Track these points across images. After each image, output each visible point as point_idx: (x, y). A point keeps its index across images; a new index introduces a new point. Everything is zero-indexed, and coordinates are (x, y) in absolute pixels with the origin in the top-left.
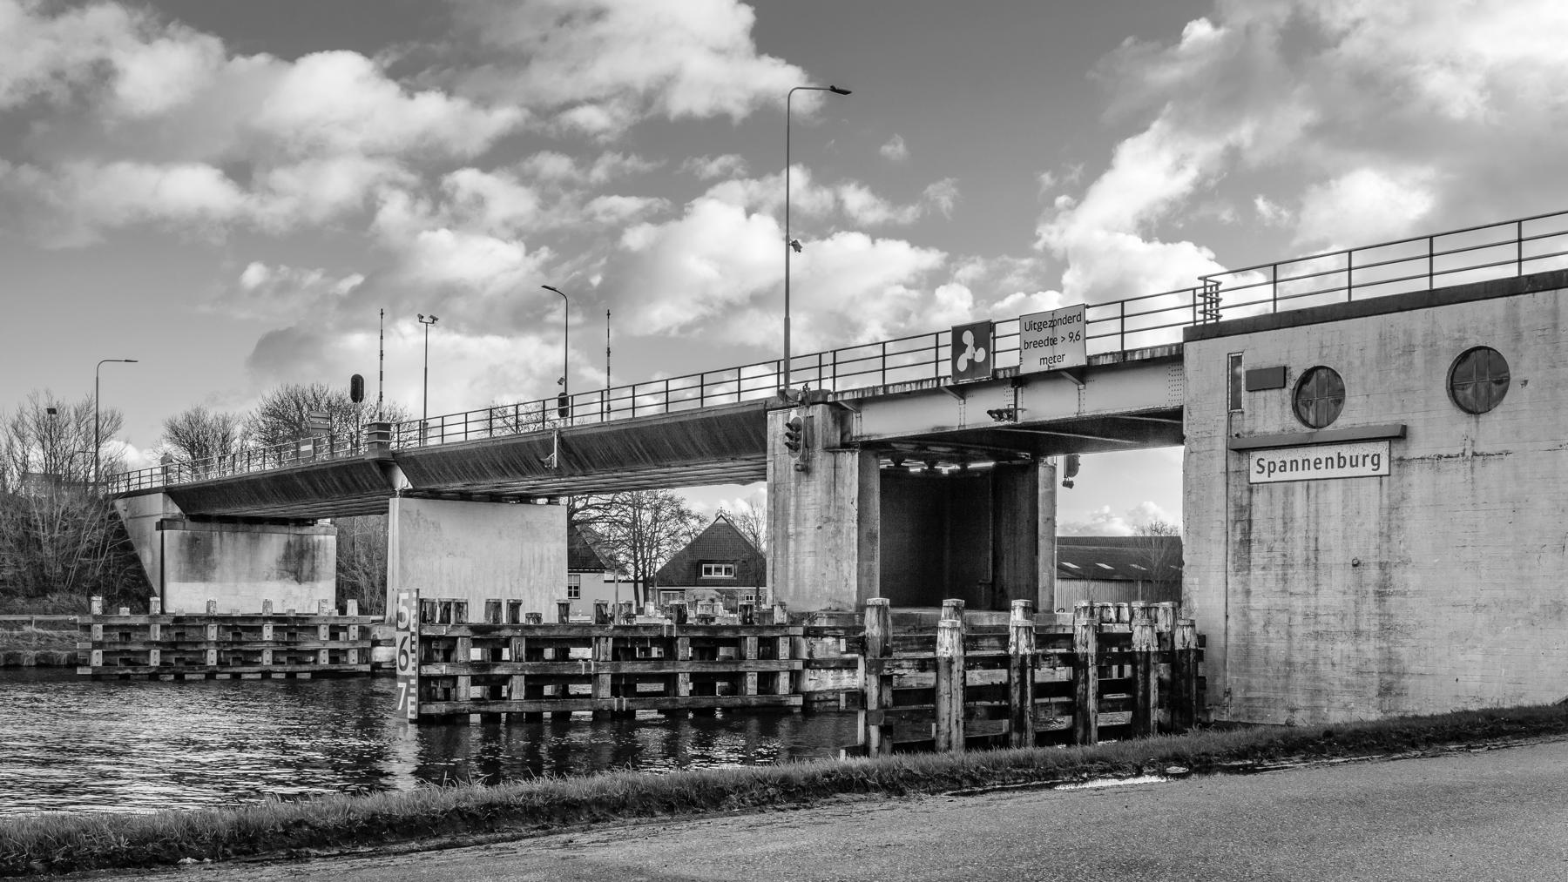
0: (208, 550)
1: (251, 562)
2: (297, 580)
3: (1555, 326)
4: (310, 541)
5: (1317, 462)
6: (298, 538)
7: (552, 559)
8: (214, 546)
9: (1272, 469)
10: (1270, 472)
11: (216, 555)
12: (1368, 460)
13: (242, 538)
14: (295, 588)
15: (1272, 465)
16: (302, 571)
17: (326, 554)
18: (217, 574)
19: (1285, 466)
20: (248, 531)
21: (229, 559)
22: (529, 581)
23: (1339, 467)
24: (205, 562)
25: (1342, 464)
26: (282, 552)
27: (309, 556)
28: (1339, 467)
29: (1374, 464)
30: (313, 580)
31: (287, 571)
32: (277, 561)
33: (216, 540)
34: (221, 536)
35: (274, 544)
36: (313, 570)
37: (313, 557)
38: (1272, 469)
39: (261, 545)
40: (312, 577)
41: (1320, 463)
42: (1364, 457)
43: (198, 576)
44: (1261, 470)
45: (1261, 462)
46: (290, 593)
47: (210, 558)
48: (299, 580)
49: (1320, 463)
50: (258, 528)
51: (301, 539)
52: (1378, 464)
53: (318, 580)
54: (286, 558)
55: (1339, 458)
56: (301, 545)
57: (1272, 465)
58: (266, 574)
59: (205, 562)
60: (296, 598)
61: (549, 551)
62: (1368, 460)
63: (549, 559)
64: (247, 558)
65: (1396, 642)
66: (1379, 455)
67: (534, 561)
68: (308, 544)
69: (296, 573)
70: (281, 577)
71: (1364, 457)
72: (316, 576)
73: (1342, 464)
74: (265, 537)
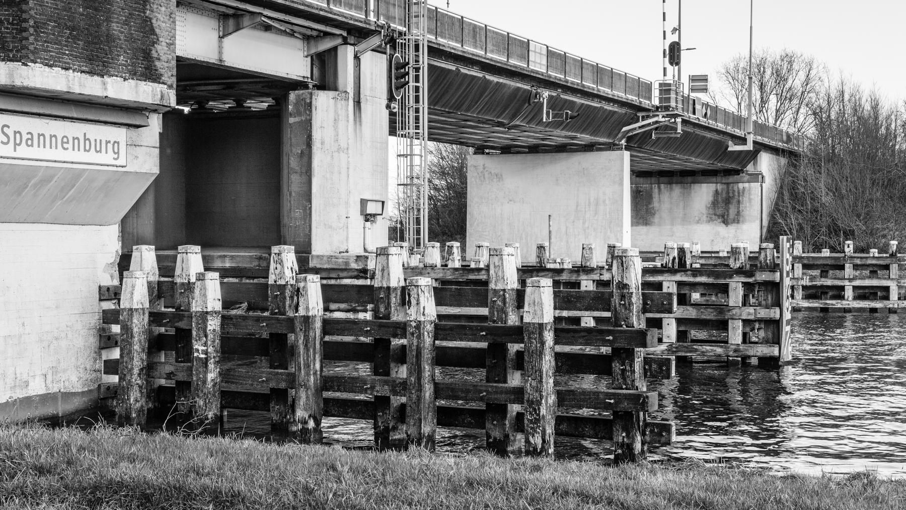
0: (650, 197)
1: (684, 208)
2: (724, 222)
3: (347, 239)
4: (736, 188)
5: (65, 140)
6: (725, 186)
7: (607, 202)
8: (654, 196)
9: (18, 141)
10: (15, 144)
11: (655, 204)
12: (110, 146)
13: (677, 190)
14: (722, 229)
15: (18, 135)
16: (728, 215)
17: (750, 200)
18: (656, 219)
19: (32, 139)
20: (681, 183)
21: (665, 206)
22: (584, 223)
23: (85, 150)
24: (647, 210)
25: (87, 148)
26: (711, 199)
27: (735, 201)
28: (85, 150)
29: (115, 153)
30: (738, 222)
31: (715, 215)
32: (706, 206)
33: (656, 190)
34: (659, 188)
35: (704, 193)
36: (738, 213)
37: (739, 202)
38: (18, 141)
39: (693, 194)
40: (737, 219)
41: (68, 143)
42: (107, 142)
43: (641, 221)
44: (5, 140)
45: (5, 129)
46: (717, 234)
47: (651, 206)
48: (726, 222)
49: (68, 143)
50: (689, 179)
51: (728, 187)
52: (118, 153)
53: (743, 222)
54: (715, 204)
55: (85, 140)
56: (728, 193)
57: (18, 135)
58: (697, 218)
59: (647, 210)
60: (724, 238)
61: (604, 194)
62: (110, 146)
63: (604, 201)
64: (681, 204)
65: (424, 435)
66: (118, 143)
67: (589, 205)
68: (734, 191)
69: (723, 216)
70: (710, 220)
71: (107, 142)
72: (741, 219)
73: (87, 148)
74: (696, 187)
